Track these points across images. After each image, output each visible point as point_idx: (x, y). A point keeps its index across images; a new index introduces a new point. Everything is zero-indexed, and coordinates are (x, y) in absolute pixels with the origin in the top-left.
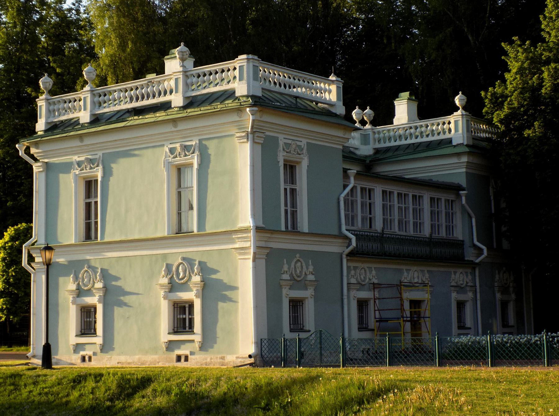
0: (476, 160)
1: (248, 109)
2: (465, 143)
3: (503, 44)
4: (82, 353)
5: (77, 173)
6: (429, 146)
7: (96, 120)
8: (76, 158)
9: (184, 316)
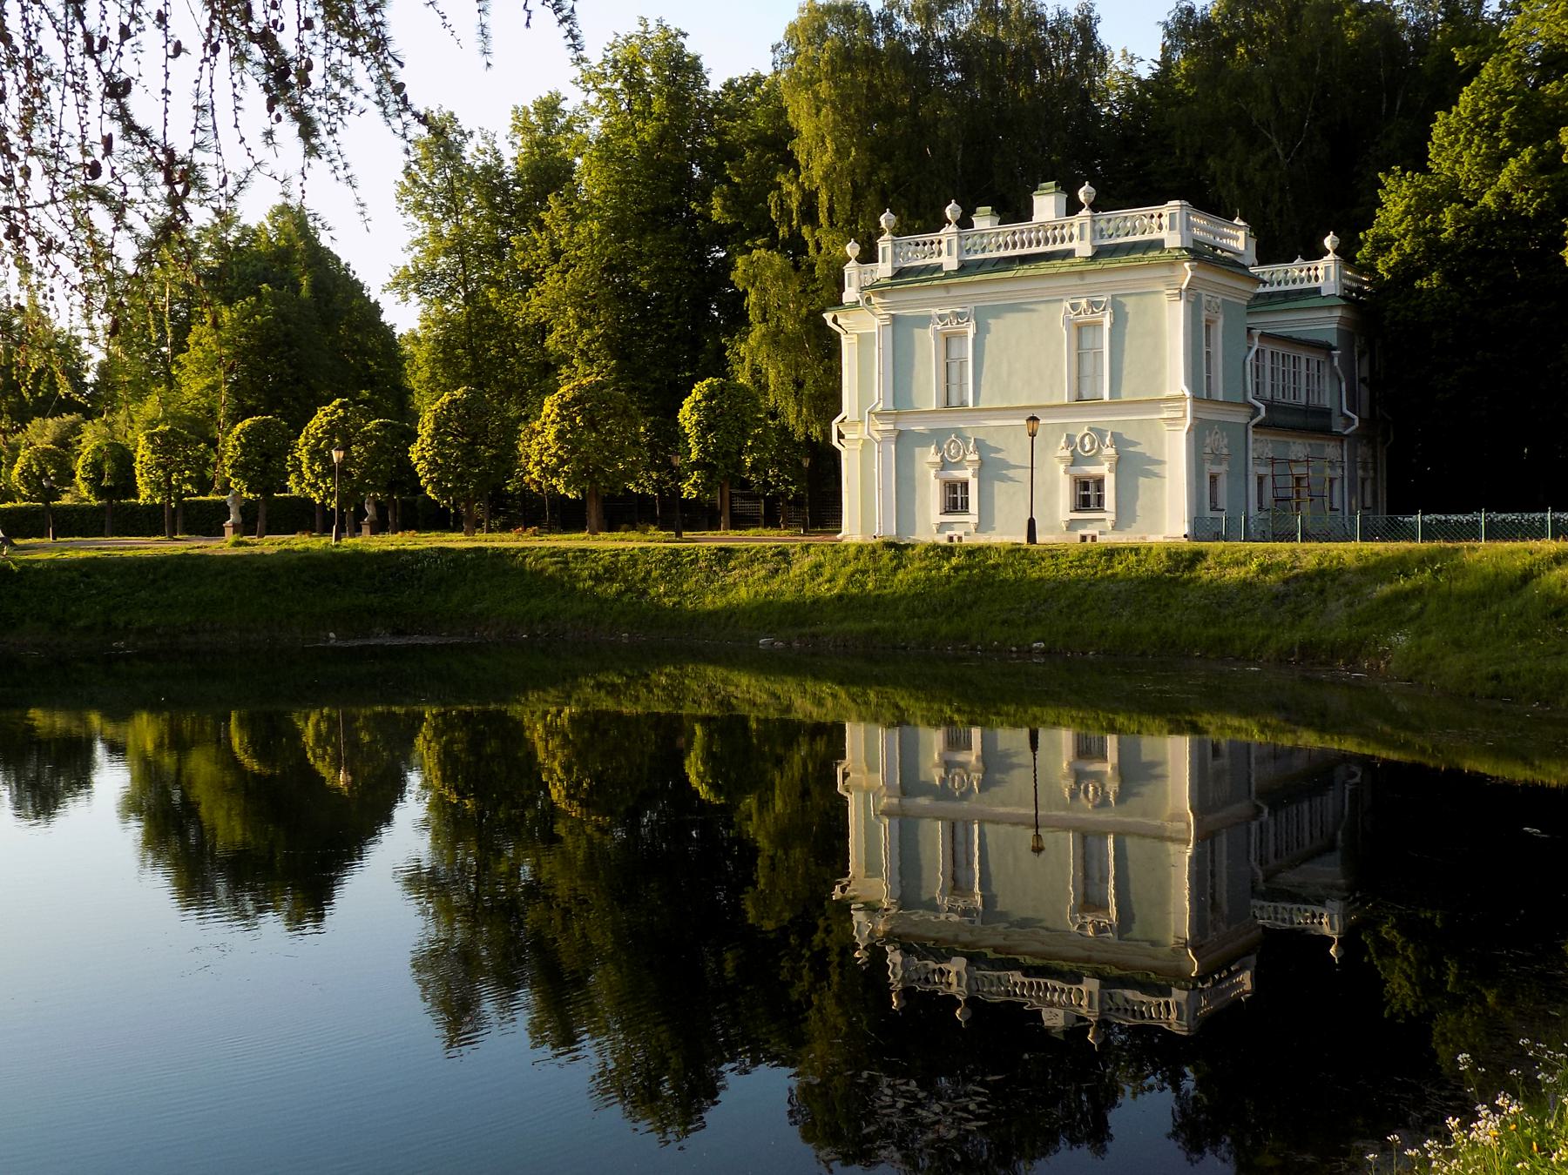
0: (1347, 315)
1: (1187, 265)
7: (965, 268)
8: (936, 311)
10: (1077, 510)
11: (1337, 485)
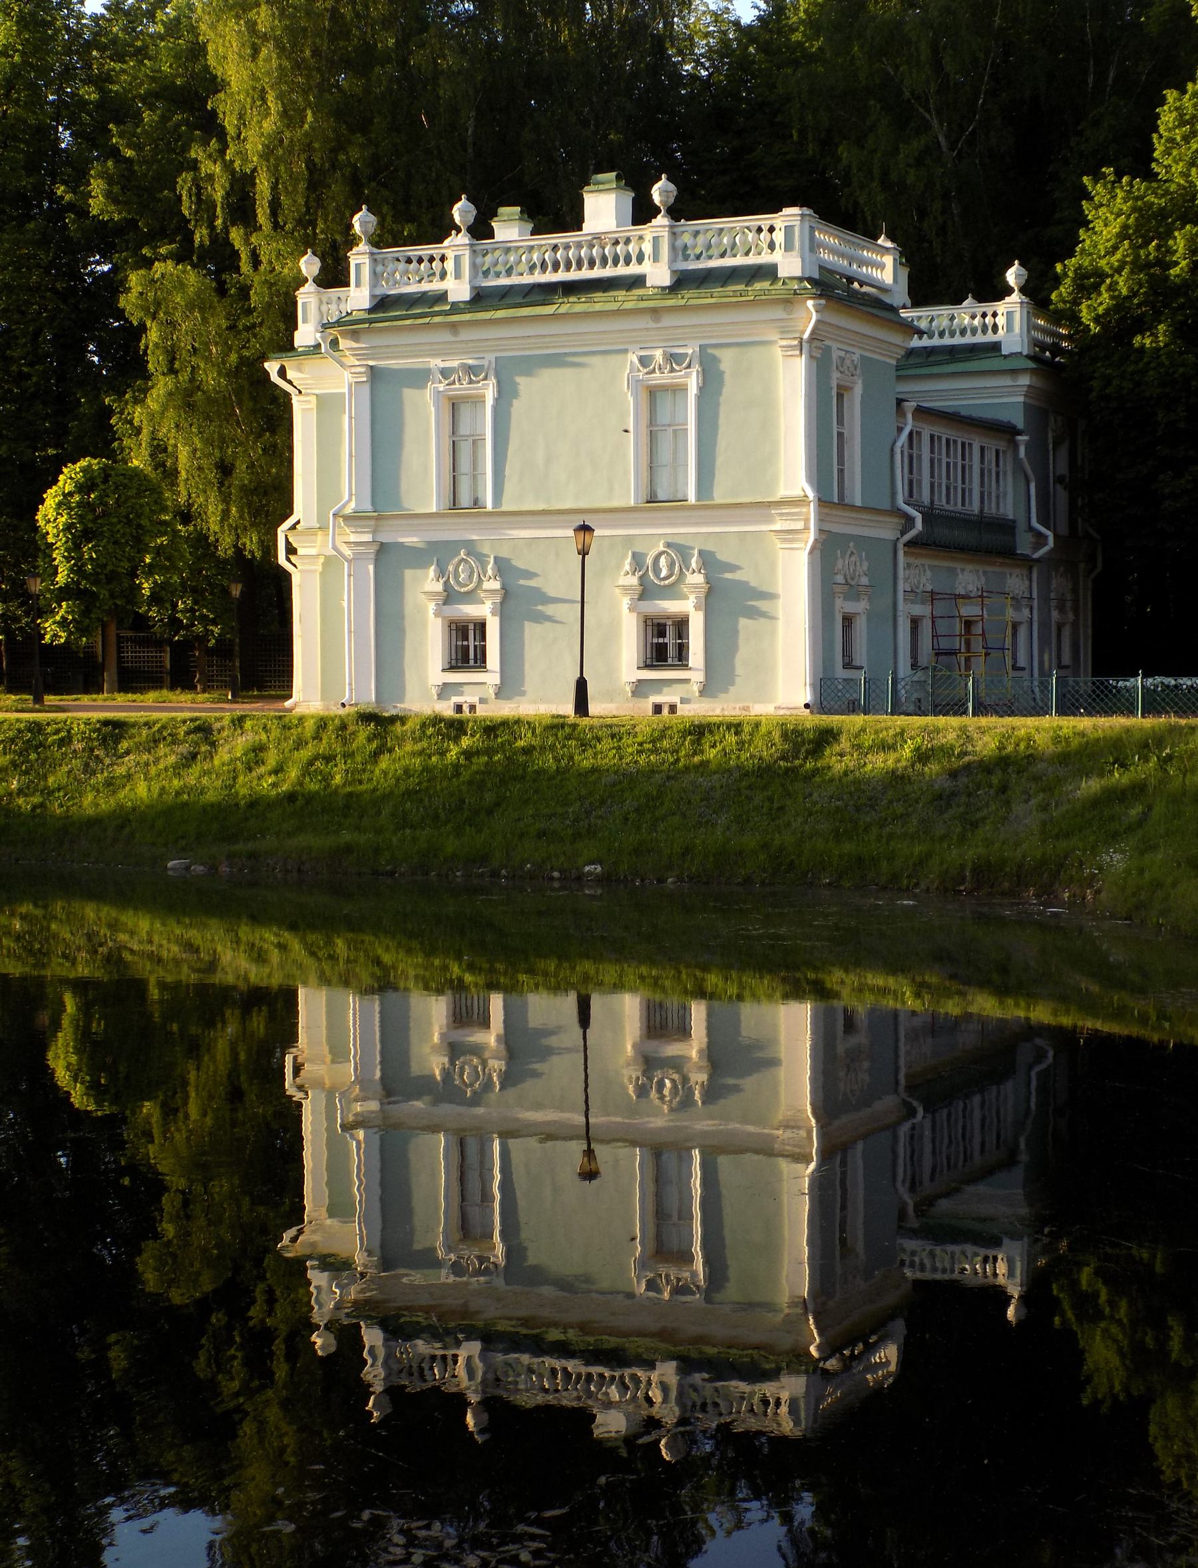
1: (810, 303)
2: (1025, 352)
3: (1085, 179)
4: (456, 699)
5: (441, 389)
7: (481, 298)
8: (436, 363)
9: (465, 643)
11: (1023, 632)
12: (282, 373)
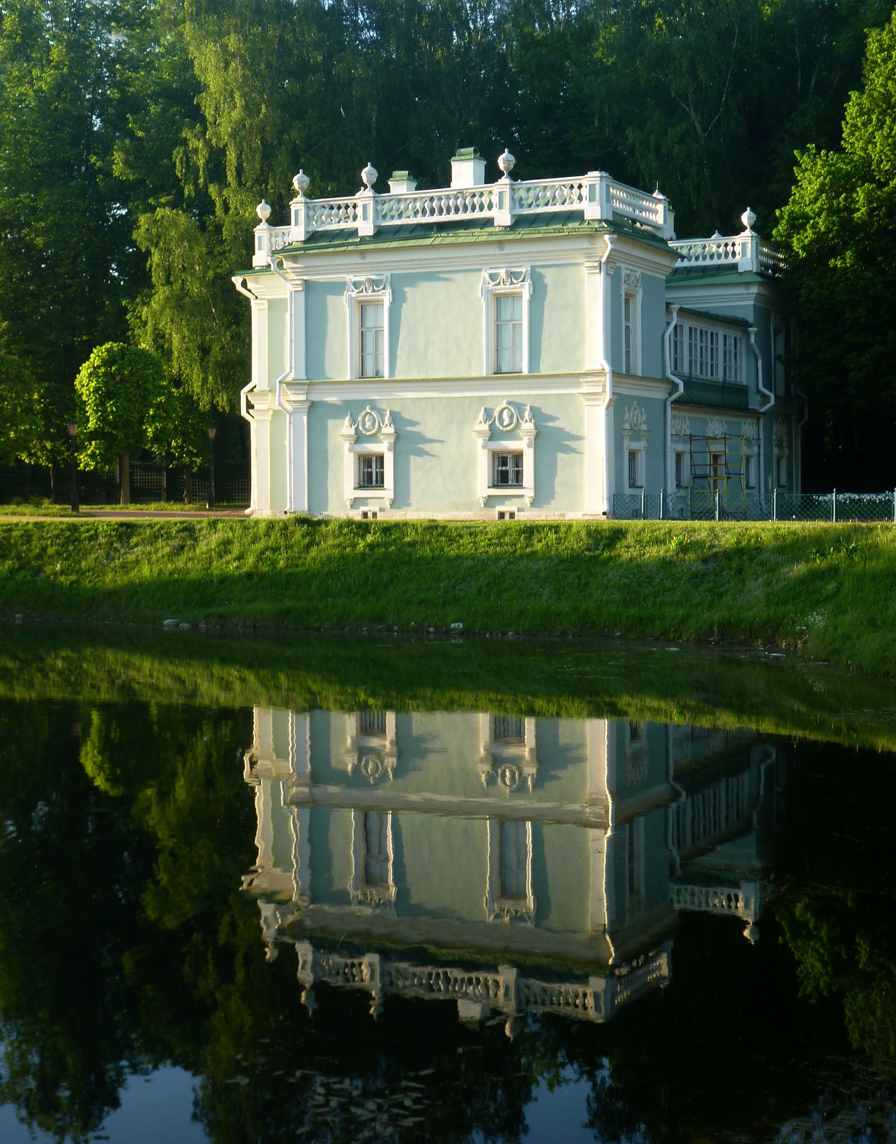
1: (607, 237)
6: (705, 271)
7: (381, 234)
8: (350, 278)
9: (370, 470)
10: (495, 486)
12: (244, 284)
